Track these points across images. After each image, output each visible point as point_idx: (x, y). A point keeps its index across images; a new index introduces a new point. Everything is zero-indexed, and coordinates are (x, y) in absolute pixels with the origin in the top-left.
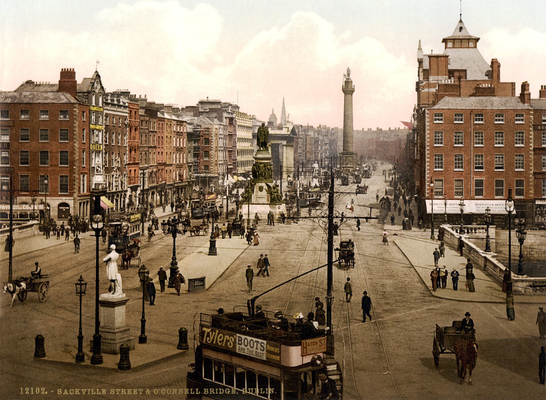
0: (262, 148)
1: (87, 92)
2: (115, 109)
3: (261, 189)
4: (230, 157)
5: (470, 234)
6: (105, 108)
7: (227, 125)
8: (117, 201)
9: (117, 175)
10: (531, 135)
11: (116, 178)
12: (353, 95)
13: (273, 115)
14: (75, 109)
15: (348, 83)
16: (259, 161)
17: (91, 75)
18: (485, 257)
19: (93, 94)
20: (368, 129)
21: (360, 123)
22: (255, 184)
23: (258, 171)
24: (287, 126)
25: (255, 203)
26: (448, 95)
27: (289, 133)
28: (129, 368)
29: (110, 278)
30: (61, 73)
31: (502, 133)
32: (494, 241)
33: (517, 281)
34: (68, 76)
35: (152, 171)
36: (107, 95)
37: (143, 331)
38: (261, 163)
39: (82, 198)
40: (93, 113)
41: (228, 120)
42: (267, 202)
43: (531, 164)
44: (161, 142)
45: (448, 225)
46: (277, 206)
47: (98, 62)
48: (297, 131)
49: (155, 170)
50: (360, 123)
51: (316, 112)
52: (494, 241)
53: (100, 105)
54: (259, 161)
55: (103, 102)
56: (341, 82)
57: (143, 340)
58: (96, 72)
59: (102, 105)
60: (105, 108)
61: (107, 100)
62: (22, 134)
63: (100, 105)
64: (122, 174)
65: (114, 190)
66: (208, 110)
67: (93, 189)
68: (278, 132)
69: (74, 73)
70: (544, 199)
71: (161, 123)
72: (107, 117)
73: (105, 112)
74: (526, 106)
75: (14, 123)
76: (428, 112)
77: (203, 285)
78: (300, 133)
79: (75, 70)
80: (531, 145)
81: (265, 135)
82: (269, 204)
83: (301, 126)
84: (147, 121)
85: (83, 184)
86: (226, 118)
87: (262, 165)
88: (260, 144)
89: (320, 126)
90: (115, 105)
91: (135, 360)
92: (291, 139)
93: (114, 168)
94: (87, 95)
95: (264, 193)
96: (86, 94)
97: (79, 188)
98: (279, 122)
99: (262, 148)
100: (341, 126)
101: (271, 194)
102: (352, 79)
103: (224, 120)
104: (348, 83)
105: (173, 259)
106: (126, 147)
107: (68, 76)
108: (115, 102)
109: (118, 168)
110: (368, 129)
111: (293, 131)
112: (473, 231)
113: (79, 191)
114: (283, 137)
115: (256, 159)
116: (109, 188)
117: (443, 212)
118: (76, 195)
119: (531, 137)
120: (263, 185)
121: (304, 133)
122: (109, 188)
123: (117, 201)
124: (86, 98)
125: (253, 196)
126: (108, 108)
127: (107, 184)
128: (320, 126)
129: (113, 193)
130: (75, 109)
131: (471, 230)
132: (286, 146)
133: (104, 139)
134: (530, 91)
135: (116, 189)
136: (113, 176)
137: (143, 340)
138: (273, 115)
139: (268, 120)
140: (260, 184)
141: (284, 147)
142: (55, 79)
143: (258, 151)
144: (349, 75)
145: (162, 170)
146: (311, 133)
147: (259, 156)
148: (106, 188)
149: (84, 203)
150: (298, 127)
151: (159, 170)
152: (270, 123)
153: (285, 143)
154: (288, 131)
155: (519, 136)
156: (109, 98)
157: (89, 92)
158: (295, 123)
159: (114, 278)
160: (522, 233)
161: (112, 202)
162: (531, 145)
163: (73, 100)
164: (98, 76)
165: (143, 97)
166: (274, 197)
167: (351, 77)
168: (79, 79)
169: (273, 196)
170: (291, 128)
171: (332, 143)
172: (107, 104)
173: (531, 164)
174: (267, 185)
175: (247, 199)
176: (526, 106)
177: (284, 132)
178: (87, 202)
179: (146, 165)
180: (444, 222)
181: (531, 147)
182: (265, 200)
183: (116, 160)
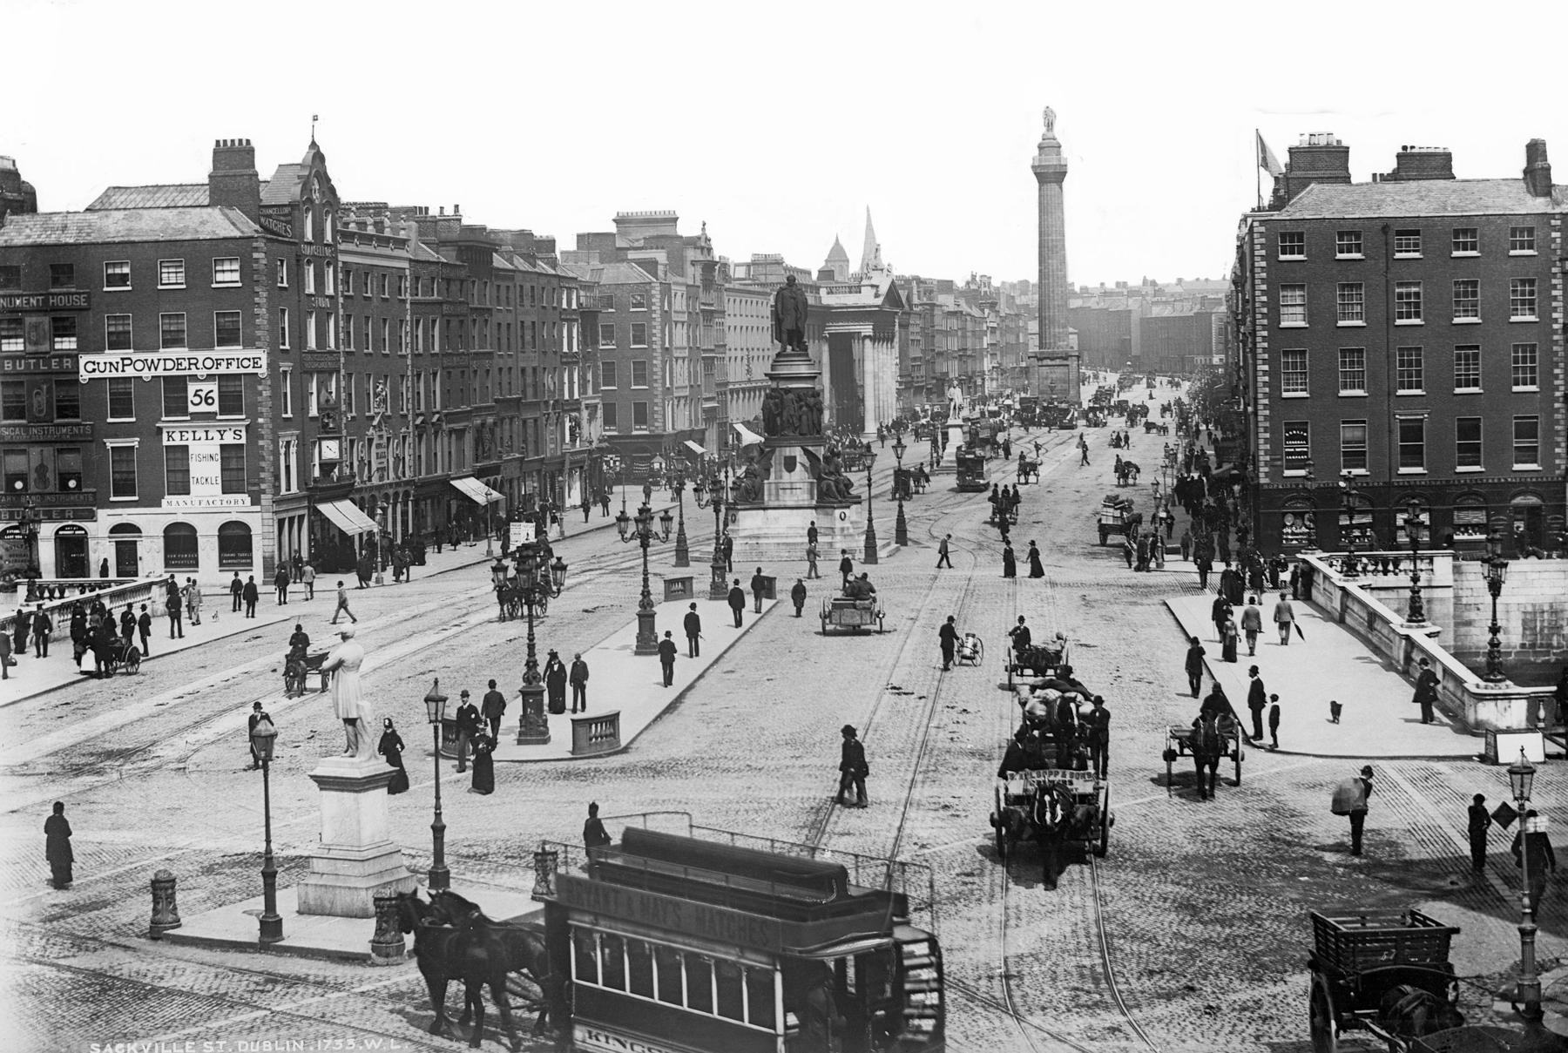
1: (289, 205)
2: (387, 251)
3: (790, 464)
5: (1391, 575)
6: (342, 247)
7: (698, 283)
8: (384, 510)
9: (381, 437)
10: (1555, 287)
11: (379, 446)
12: (1065, 184)
13: (838, 254)
14: (255, 255)
15: (1049, 146)
16: (783, 385)
19: (307, 210)
20: (1118, 284)
21: (1089, 269)
22: (773, 452)
23: (780, 414)
24: (873, 282)
25: (772, 504)
26: (1321, 180)
27: (879, 301)
30: (215, 152)
31: (1474, 284)
32: (1449, 593)
33: (1481, 698)
34: (233, 160)
35: (483, 425)
36: (347, 209)
38: (788, 391)
40: (309, 263)
42: (806, 503)
43: (1557, 371)
44: (504, 341)
45: (1320, 554)
46: (837, 512)
47: (315, 118)
48: (903, 294)
49: (490, 420)
50: (1089, 269)
51: (964, 239)
52: (1449, 593)
53: (329, 238)
54: (783, 385)
58: (314, 145)
59: (334, 238)
60: (342, 247)
61: (346, 224)
62: (112, 329)
63: (329, 238)
64: (396, 436)
65: (375, 481)
66: (641, 243)
67: (315, 480)
68: (851, 300)
69: (252, 150)
70: (3, 297)
71: (503, 284)
72: (348, 273)
73: (342, 258)
75: (88, 300)
76: (1263, 229)
77: (615, 735)
78: (915, 300)
79: (253, 144)
80: (1555, 315)
82: (815, 508)
83: (919, 281)
84: (462, 281)
85: (288, 467)
86: (693, 263)
87: (791, 396)
88: (785, 337)
89: (974, 277)
90: (370, 238)
93: (372, 418)
94: (290, 214)
95: (800, 475)
96: (287, 210)
97: (277, 478)
98: (855, 267)
99: (789, 348)
100: (1034, 278)
101: (820, 479)
102: (1060, 140)
103: (690, 270)
104: (1049, 146)
105: (527, 664)
106: (405, 357)
107: (233, 160)
108: (371, 230)
109: (385, 419)
110: (1118, 284)
111: (893, 295)
112: (1391, 567)
113: (277, 488)
114: (860, 314)
116: (361, 477)
118: (266, 499)
119: (1554, 293)
120: (797, 452)
121: (925, 300)
122: (361, 477)
123: (384, 510)
124: (288, 222)
126: (351, 247)
127: (356, 464)
128: (974, 277)
129: (371, 488)
130: (255, 255)
131: (1385, 565)
132: (873, 339)
133: (341, 336)
134: (1550, 160)
135: (381, 478)
136: (370, 441)
138: (838, 254)
139: (821, 264)
140: (788, 452)
141: (868, 342)
142: (199, 170)
143: (778, 355)
144: (1050, 125)
145: (511, 419)
146: (947, 301)
147: (783, 371)
149: (291, 520)
150: (908, 281)
151: (502, 420)
152: (826, 274)
153: (867, 329)
154: (877, 296)
155: (1523, 293)
157: (293, 206)
158: (896, 272)
159: (353, 715)
160: (1496, 566)
161: (372, 515)
162: (1555, 315)
164: (318, 157)
165: (449, 212)
166: (829, 486)
168: (265, 168)
169: (824, 484)
170: (884, 289)
171: (1009, 324)
172: (349, 237)
173: (1557, 371)
174: (807, 452)
175: (751, 496)
176: (1539, 205)
177: (866, 298)
178: (301, 518)
181: (1556, 321)
182: (802, 497)
183: (376, 395)
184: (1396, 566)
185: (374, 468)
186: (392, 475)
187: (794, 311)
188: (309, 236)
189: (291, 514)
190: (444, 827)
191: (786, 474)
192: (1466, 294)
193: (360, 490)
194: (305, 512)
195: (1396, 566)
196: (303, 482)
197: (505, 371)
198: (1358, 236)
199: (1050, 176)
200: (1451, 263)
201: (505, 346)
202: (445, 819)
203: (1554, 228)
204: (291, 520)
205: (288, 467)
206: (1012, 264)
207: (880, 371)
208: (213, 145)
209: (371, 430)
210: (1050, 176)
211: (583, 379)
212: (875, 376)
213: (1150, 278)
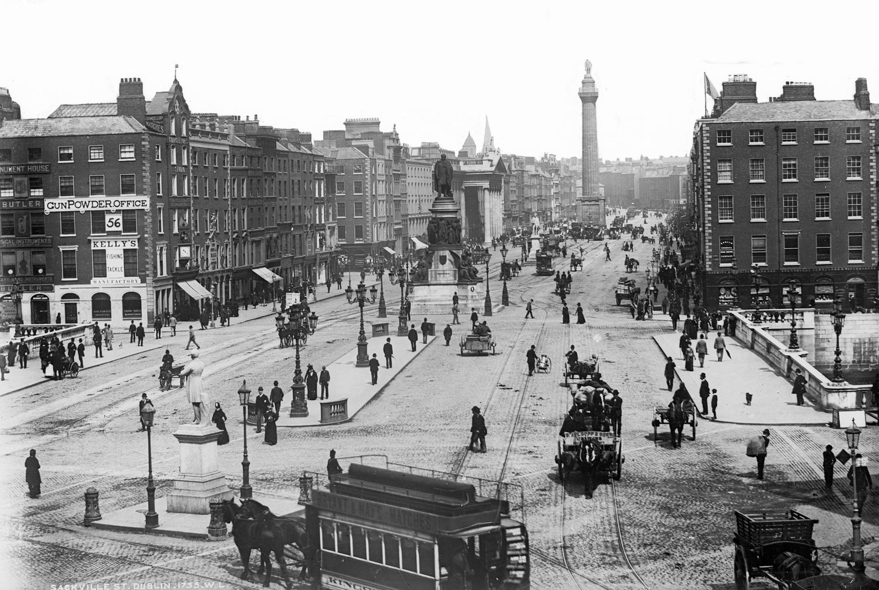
0: (442, 195)
2: (217, 141)
3: (443, 260)
4: (397, 210)
5: (780, 322)
6: (192, 138)
7: (391, 158)
8: (215, 286)
9: (213, 245)
10: (871, 161)
11: (212, 250)
12: (597, 103)
13: (470, 142)
14: (143, 143)
15: (588, 82)
16: (439, 216)
19: (172, 118)
20: (627, 159)
21: (611, 151)
22: (433, 253)
23: (437, 232)
24: (489, 158)
25: (433, 282)
26: (741, 101)
27: (493, 169)
30: (121, 85)
31: (827, 159)
33: (830, 391)
34: (131, 90)
35: (271, 238)
36: (194, 117)
38: (442, 219)
39: (159, 284)
40: (173, 147)
42: (452, 282)
43: (873, 208)
44: (283, 191)
45: (740, 310)
46: (469, 287)
48: (506, 165)
49: (275, 235)
50: (611, 151)
51: (536, 131)
52: (812, 332)
53: (184, 133)
54: (439, 216)
55: (188, 130)
59: (187, 133)
60: (192, 138)
61: (194, 126)
62: (63, 184)
63: (184, 133)
64: (222, 244)
65: (210, 270)
66: (360, 136)
68: (477, 168)
69: (141, 84)
70: (2, 166)
71: (282, 159)
72: (195, 153)
73: (192, 144)
75: (49, 168)
76: (708, 128)
77: (345, 412)
78: (513, 168)
79: (142, 81)
80: (872, 177)
81: (447, 174)
82: (457, 285)
83: (515, 157)
85: (161, 262)
86: (389, 147)
87: (443, 222)
88: (440, 189)
89: (546, 155)
90: (207, 133)
93: (209, 234)
94: (162, 120)
95: (448, 266)
96: (161, 118)
97: (155, 268)
99: (442, 195)
100: (580, 156)
101: (460, 268)
102: (594, 79)
103: (387, 151)
104: (588, 82)
105: (296, 372)
106: (227, 200)
107: (131, 90)
108: (208, 129)
110: (627, 159)
111: (500, 165)
112: (780, 318)
113: (155, 274)
114: (482, 176)
116: (202, 267)
118: (149, 280)
119: (871, 164)
120: (447, 253)
121: (518, 168)
123: (215, 286)
124: (161, 125)
126: (197, 138)
127: (199, 260)
128: (546, 155)
129: (208, 274)
130: (143, 143)
131: (777, 317)
132: (490, 190)
133: (191, 188)
134: (869, 89)
135: (214, 268)
136: (208, 247)
138: (470, 142)
139: (460, 148)
140: (442, 253)
141: (487, 192)
142: (112, 95)
143: (436, 199)
145: (287, 235)
146: (531, 169)
148: (198, 267)
149: (163, 291)
150: (509, 158)
151: (282, 235)
152: (463, 154)
153: (486, 185)
154: (491, 166)
155: (854, 164)
157: (164, 115)
158: (502, 153)
159: (198, 401)
160: (838, 317)
161: (208, 289)
162: (872, 177)
164: (178, 88)
165: (252, 119)
166: (465, 272)
168: (149, 94)
169: (462, 272)
170: (495, 162)
171: (566, 181)
172: (195, 133)
173: (873, 208)
174: (452, 253)
175: (421, 278)
176: (863, 115)
177: (486, 167)
178: (169, 290)
179: (260, 228)
181: (872, 180)
182: (450, 278)
183: (211, 221)
184: (783, 317)
185: (210, 262)
186: (220, 266)
187: (445, 174)
188: (173, 132)
189: (163, 288)
191: (440, 266)
192: (822, 165)
193: (202, 275)
194: (171, 287)
195: (783, 317)
196: (170, 270)
197: (283, 207)
198: (761, 132)
200: (814, 147)
203: (871, 128)
204: (163, 291)
205: (161, 262)
206: (567, 148)
207: (493, 208)
208: (119, 81)
209: (208, 241)
210: (589, 99)
212: (491, 211)
213: (644, 156)
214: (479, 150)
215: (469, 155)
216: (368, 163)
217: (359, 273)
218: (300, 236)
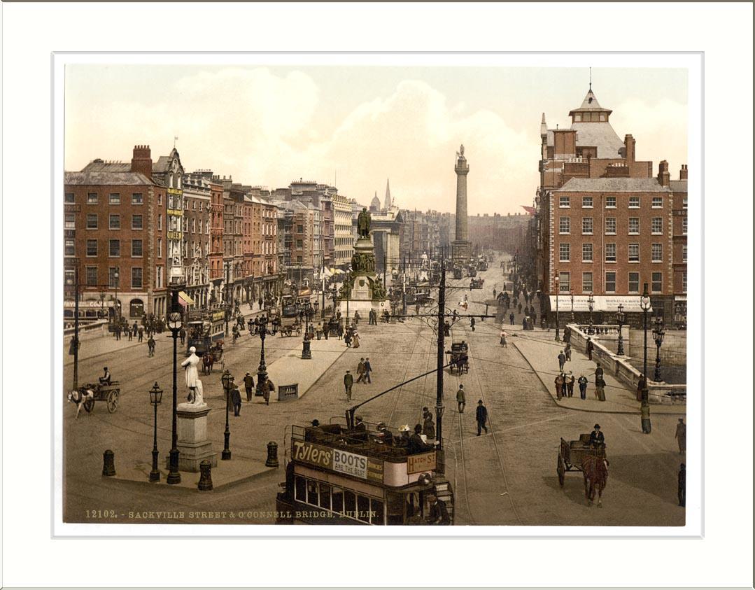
2: (196, 192)
3: (362, 283)
4: (327, 246)
5: (600, 335)
6: (185, 190)
8: (197, 297)
11: (196, 270)
13: (376, 199)
14: (150, 192)
16: (360, 251)
17: (168, 153)
18: (617, 362)
19: (171, 175)
20: (485, 215)
23: (359, 263)
25: (355, 299)
27: (394, 219)
28: (210, 487)
29: (189, 386)
32: (628, 342)
34: (142, 154)
35: (238, 263)
36: (187, 175)
37: (227, 446)
38: (361, 254)
41: (324, 204)
42: (368, 299)
43: (670, 255)
46: (380, 303)
47: (176, 138)
48: (403, 217)
49: (241, 261)
50: (472, 210)
51: (427, 195)
52: (628, 342)
53: (179, 187)
54: (360, 251)
55: (182, 184)
56: (453, 161)
57: (226, 456)
58: (174, 149)
60: (185, 190)
61: (187, 182)
63: (179, 187)
64: (203, 267)
65: (194, 284)
68: (382, 218)
69: (150, 151)
71: (248, 207)
72: (186, 201)
73: (185, 195)
74: (665, 188)
76: (553, 195)
77: (296, 393)
85: (159, 278)
86: (322, 202)
87: (363, 256)
88: (361, 232)
89: (430, 211)
90: (196, 187)
91: (217, 478)
92: (396, 226)
93: (194, 259)
94: (164, 176)
95: (366, 288)
97: (155, 282)
98: (382, 206)
99: (363, 237)
101: (373, 289)
103: (321, 204)
105: (261, 363)
106: (208, 235)
107: (142, 154)
108: (196, 184)
109: (199, 259)
110: (485, 215)
111: (399, 216)
112: (604, 331)
113: (154, 286)
114: (387, 224)
115: (356, 249)
117: (570, 310)
120: (365, 278)
123: (197, 297)
125: (353, 292)
127: (187, 277)
128: (430, 211)
129: (193, 287)
130: (150, 192)
131: (602, 331)
132: (391, 234)
133: (183, 226)
135: (197, 284)
136: (193, 268)
137: (226, 456)
138: (376, 199)
139: (370, 205)
140: (361, 278)
141: (389, 236)
142: (128, 158)
143: (358, 240)
144: (462, 153)
145: (249, 261)
146: (419, 220)
147: (360, 245)
148: (185, 282)
149: (160, 299)
151: (245, 261)
152: (373, 208)
153: (389, 230)
154: (393, 217)
155: (657, 223)
156: (189, 179)
157: (165, 173)
161: (192, 298)
162: (670, 233)
163: (148, 182)
165: (227, 178)
167: (465, 155)
168: (155, 158)
169: (375, 292)
170: (396, 214)
171: (443, 230)
173: (670, 255)
174: (369, 278)
175: (346, 295)
176: (665, 188)
177: (388, 218)
178: (164, 298)
180: (571, 321)
181: (670, 235)
182: (366, 296)
183: (196, 250)
184: (606, 331)
185: (194, 280)
186: (201, 282)
187: (364, 224)
188: (171, 186)
189: (160, 297)
190: (229, 434)
191: (360, 288)
192: (634, 223)
193: (187, 288)
194: (165, 296)
195: (606, 331)
196: (165, 284)
197: (247, 242)
198: (614, 199)
199: (461, 169)
200: (653, 211)
201: (247, 232)
202: (230, 431)
203: (670, 198)
204: (160, 299)
205: (159, 278)
206: (448, 207)
207: (393, 246)
208: (134, 148)
209: (193, 264)
210: (461, 169)
211: (273, 245)
212: (391, 249)
213: (497, 213)
214: (382, 206)
215: (377, 209)
216: (567, 202)
217: (594, 310)
218: (218, 262)
